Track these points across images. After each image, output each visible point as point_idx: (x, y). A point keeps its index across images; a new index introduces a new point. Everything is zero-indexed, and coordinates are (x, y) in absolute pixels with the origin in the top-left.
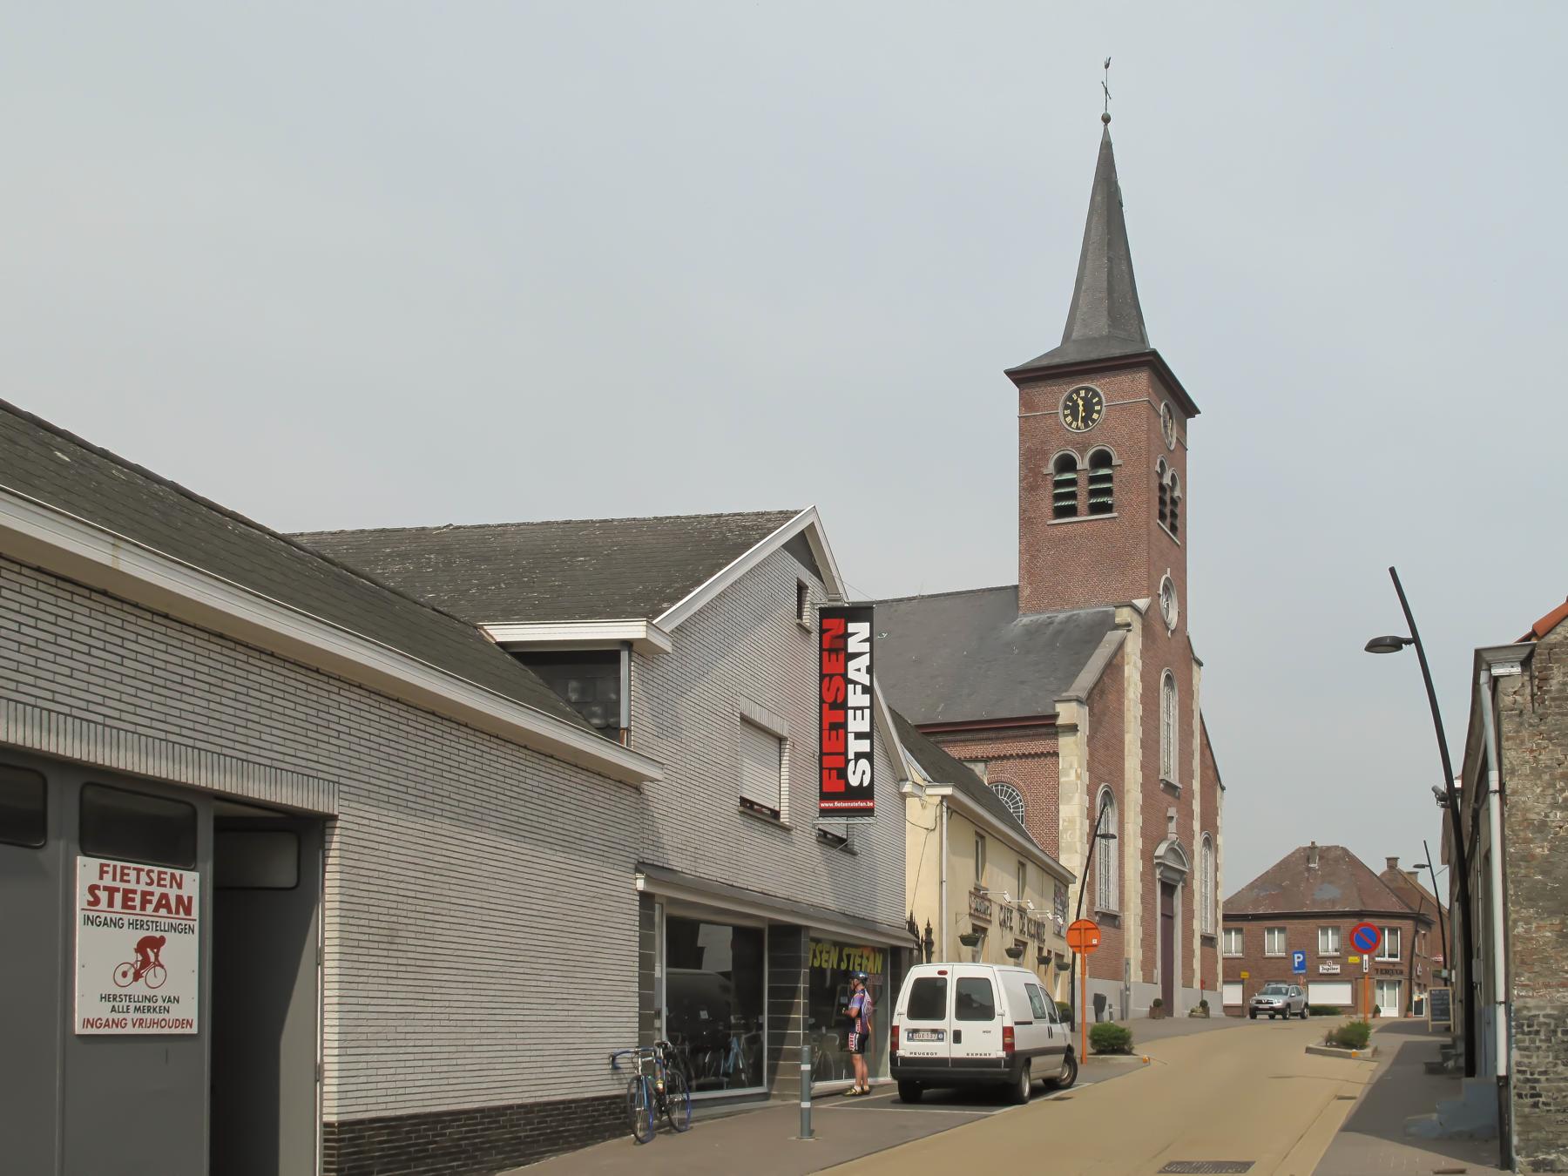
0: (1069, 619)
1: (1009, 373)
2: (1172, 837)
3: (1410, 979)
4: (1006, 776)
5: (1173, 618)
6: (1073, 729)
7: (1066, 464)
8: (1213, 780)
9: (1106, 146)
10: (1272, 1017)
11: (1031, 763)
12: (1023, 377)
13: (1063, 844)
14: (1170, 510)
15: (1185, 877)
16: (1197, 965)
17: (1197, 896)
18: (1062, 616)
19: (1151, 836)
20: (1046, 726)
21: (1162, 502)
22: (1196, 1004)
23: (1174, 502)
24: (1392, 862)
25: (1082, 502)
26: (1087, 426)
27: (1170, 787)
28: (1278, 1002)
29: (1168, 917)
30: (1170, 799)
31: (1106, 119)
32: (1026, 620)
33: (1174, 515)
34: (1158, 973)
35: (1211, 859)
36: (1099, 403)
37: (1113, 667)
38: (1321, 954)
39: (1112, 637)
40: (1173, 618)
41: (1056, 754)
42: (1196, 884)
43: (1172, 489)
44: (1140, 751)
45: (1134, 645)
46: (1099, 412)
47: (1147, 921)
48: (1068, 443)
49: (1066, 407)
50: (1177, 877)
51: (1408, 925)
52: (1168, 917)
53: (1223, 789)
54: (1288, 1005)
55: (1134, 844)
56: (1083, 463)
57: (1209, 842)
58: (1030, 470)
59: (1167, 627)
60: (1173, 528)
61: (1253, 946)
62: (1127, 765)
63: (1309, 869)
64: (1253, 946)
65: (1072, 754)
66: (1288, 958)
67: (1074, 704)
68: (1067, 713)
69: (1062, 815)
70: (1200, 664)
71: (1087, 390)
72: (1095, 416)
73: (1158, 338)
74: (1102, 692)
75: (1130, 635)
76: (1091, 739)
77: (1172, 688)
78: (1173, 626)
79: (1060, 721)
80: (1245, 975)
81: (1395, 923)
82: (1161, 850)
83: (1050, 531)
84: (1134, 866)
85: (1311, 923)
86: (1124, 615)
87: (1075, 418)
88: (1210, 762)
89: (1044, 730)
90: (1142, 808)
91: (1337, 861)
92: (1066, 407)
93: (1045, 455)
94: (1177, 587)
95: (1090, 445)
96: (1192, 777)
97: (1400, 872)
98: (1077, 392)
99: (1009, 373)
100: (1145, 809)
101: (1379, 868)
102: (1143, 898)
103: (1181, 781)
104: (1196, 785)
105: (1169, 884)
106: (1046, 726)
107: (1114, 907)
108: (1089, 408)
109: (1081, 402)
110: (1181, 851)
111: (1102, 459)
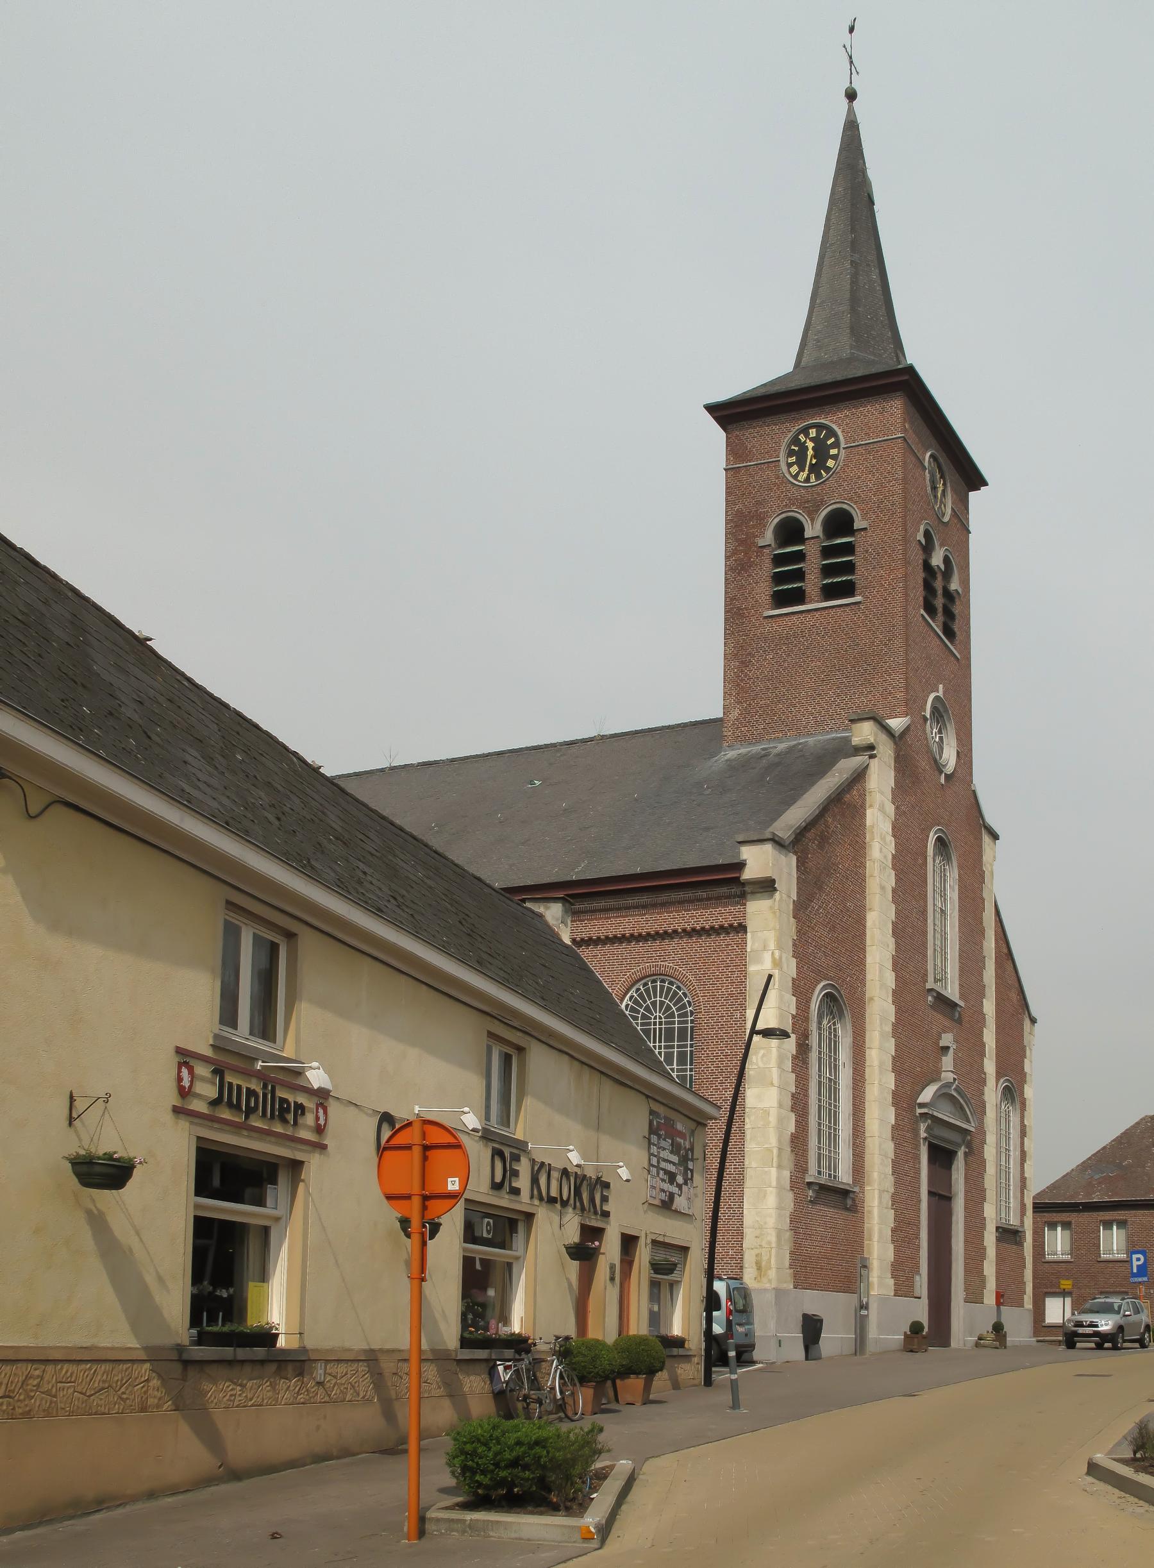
0: (790, 750)
1: (711, 409)
2: (948, 1077)
4: (668, 965)
5: (949, 757)
6: (767, 886)
7: (791, 531)
8: (1016, 1008)
9: (851, 129)
10: (1100, 1346)
11: (705, 942)
12: (731, 414)
14: (943, 602)
15: (972, 1143)
16: (989, 1269)
17: (991, 1169)
18: (782, 746)
19: (910, 1071)
20: (725, 882)
22: (986, 1327)
23: (949, 596)
25: (813, 582)
26: (819, 476)
27: (943, 1002)
28: (1106, 1324)
29: (941, 1199)
30: (947, 1023)
31: (851, 95)
32: (731, 754)
33: (949, 614)
34: (922, 1283)
35: (1014, 1119)
36: (836, 445)
37: (846, 804)
39: (846, 766)
41: (742, 928)
42: (990, 1152)
43: (947, 574)
44: (891, 942)
45: (881, 780)
46: (835, 457)
47: (902, 1201)
49: (791, 453)
52: (941, 1199)
53: (1033, 1021)
54: (1121, 1328)
55: (881, 1082)
56: (813, 529)
57: (1013, 1094)
58: (742, 542)
59: (939, 768)
60: (949, 633)
61: (1085, 1245)
64: (1085, 1245)
65: (768, 936)
67: (768, 847)
68: (758, 861)
70: (995, 837)
71: (820, 427)
72: (830, 463)
73: (919, 353)
74: (824, 840)
75: (874, 764)
76: (801, 908)
77: (947, 858)
78: (949, 769)
79: (748, 874)
80: (1066, 1284)
82: (927, 1095)
83: (768, 627)
84: (880, 1117)
86: (865, 732)
88: (1012, 980)
89: (724, 890)
90: (895, 1026)
92: (791, 453)
93: (761, 520)
94: (955, 711)
95: (822, 502)
96: (982, 995)
98: (805, 430)
99: (711, 409)
100: (899, 1028)
102: (895, 1164)
103: (962, 996)
104: (989, 1007)
105: (942, 1149)
106: (725, 882)
107: (844, 1176)
108: (822, 452)
109: (810, 445)
110: (964, 1097)
111: (840, 523)
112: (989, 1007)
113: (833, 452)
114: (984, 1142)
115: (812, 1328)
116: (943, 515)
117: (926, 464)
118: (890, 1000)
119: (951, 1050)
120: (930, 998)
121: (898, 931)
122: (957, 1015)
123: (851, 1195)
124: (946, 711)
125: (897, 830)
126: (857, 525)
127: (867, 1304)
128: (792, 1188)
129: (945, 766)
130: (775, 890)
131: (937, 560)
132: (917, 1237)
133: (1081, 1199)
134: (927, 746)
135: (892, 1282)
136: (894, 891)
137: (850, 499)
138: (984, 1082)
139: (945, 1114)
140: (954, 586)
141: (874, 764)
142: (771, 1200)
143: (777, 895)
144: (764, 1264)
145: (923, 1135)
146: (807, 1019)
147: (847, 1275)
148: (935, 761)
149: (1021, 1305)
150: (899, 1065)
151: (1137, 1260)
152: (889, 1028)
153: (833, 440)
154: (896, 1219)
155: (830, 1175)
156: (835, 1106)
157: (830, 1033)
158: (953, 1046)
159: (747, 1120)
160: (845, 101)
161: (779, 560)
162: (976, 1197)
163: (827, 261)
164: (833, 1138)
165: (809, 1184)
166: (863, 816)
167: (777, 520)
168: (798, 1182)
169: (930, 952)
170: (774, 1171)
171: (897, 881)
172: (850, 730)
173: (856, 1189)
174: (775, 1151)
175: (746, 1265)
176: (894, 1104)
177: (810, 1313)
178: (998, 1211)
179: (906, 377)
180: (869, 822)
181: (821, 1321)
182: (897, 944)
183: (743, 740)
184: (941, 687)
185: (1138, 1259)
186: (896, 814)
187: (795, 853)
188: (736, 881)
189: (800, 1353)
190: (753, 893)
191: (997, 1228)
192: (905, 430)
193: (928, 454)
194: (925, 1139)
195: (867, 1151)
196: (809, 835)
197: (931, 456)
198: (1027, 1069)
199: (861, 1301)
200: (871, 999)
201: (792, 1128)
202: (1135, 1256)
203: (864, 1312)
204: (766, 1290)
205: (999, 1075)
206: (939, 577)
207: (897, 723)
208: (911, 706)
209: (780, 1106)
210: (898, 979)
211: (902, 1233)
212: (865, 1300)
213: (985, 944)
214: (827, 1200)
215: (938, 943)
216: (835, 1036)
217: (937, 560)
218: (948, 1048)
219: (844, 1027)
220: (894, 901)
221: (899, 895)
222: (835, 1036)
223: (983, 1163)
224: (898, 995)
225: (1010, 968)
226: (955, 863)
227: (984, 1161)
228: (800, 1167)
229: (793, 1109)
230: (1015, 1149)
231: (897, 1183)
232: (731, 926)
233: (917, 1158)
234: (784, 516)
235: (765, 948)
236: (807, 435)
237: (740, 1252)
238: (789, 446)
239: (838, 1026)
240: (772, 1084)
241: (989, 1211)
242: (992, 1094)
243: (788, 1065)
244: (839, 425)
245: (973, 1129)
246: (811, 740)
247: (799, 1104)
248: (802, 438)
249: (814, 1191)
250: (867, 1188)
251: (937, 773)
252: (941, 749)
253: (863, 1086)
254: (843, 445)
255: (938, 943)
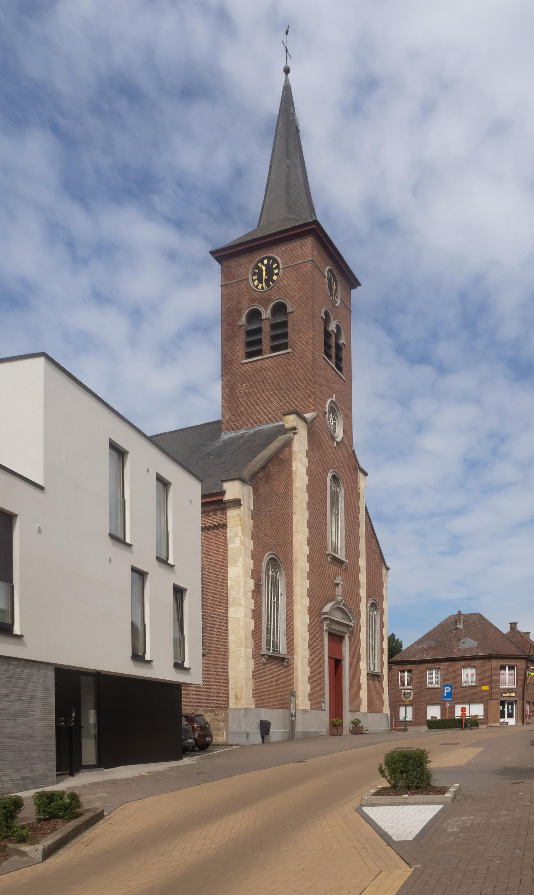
0: (256, 433)
3: (523, 699)
5: (339, 434)
6: (237, 503)
7: (254, 315)
8: (378, 561)
9: (287, 89)
13: (230, 600)
14: (336, 351)
15: (354, 632)
16: (363, 694)
18: (251, 431)
21: (327, 346)
24: (513, 626)
26: (268, 285)
31: (287, 71)
36: (278, 267)
37: (281, 460)
38: (464, 685)
40: (339, 434)
41: (225, 526)
42: (363, 636)
45: (300, 444)
46: (277, 274)
47: (314, 662)
48: (254, 301)
50: (344, 629)
51: (522, 663)
53: (388, 569)
56: (266, 314)
57: (376, 605)
59: (333, 439)
62: (295, 540)
63: (457, 629)
66: (441, 689)
69: (229, 575)
70: (366, 474)
71: (269, 258)
72: (275, 278)
74: (268, 479)
76: (256, 514)
78: (339, 440)
81: (513, 662)
82: (327, 608)
84: (302, 620)
85: (458, 664)
86: (291, 421)
87: (260, 282)
91: (477, 624)
93: (239, 312)
95: (270, 300)
97: (519, 632)
98: (262, 261)
100: (311, 575)
101: (505, 629)
104: (362, 562)
105: (335, 636)
107: (282, 650)
110: (349, 610)
111: (280, 309)
112: (362, 562)
113: (276, 271)
114: (360, 631)
115: (265, 728)
116: (336, 303)
117: (326, 274)
118: (306, 560)
119: (341, 585)
120: (329, 559)
121: (310, 525)
122: (344, 567)
123: (286, 660)
124: (338, 408)
125: (309, 472)
126: (289, 310)
127: (295, 714)
128: (253, 658)
129: (337, 438)
130: (241, 505)
131: (332, 327)
132: (323, 679)
133: (417, 658)
134: (327, 427)
135: (309, 703)
136: (308, 504)
137: (285, 297)
138: (359, 601)
139: (338, 617)
140: (342, 341)
141: (296, 437)
142: (242, 664)
143: (242, 507)
144: (239, 696)
145: (325, 628)
146: (260, 571)
147: (284, 699)
148: (331, 435)
149: (382, 712)
150: (311, 594)
151: (447, 690)
152: (306, 575)
153: (276, 265)
154: (311, 671)
155: (274, 651)
156: (277, 616)
157: (273, 579)
158: (341, 583)
159: (229, 624)
160: (284, 74)
161: (249, 333)
162: (356, 658)
163: (299, 171)
164: (276, 632)
165: (263, 655)
166: (291, 465)
167: (247, 311)
168: (257, 654)
169: (329, 535)
170: (243, 649)
171: (309, 498)
172: (283, 420)
173: (289, 657)
174: (244, 639)
175: (230, 697)
176: (309, 613)
177: (263, 719)
178: (368, 665)
179: (314, 226)
180: (294, 468)
181: (269, 724)
182: (310, 532)
183: (231, 429)
184: (334, 396)
185: (448, 689)
186: (309, 463)
187: (251, 485)
188: (221, 502)
189: (259, 740)
190: (229, 507)
191: (368, 674)
192: (313, 256)
193: (327, 268)
194: (327, 630)
195: (295, 637)
196: (259, 475)
197: (329, 270)
198: (384, 593)
199: (291, 713)
200: (296, 560)
201: (252, 627)
202: (446, 688)
203: (293, 718)
204: (240, 709)
205: (368, 597)
206: (333, 337)
207: (308, 416)
208: (318, 406)
209: (246, 616)
210: (310, 549)
211: (314, 679)
212: (294, 713)
213: (360, 530)
214: (272, 662)
215: (334, 530)
216: (276, 580)
217: (332, 327)
218: (339, 584)
219: (281, 575)
220: (308, 509)
221: (310, 506)
222: (276, 580)
223: (359, 642)
224: (311, 558)
225: (374, 541)
226: (342, 489)
227: (360, 641)
228: (257, 647)
229: (253, 617)
230: (378, 635)
231: (311, 653)
232: (219, 525)
233: (322, 640)
234: (250, 309)
235: (236, 536)
236: (262, 263)
237: (227, 691)
238: (253, 270)
239: (278, 574)
240: (241, 606)
241: (363, 666)
242: (363, 607)
243: (250, 595)
244: (279, 256)
245: (353, 625)
246: (266, 427)
247: (256, 615)
248: (260, 265)
249: (265, 658)
250: (295, 656)
251: (332, 442)
252: (335, 429)
253: (292, 605)
254: (281, 267)
255: (334, 530)
